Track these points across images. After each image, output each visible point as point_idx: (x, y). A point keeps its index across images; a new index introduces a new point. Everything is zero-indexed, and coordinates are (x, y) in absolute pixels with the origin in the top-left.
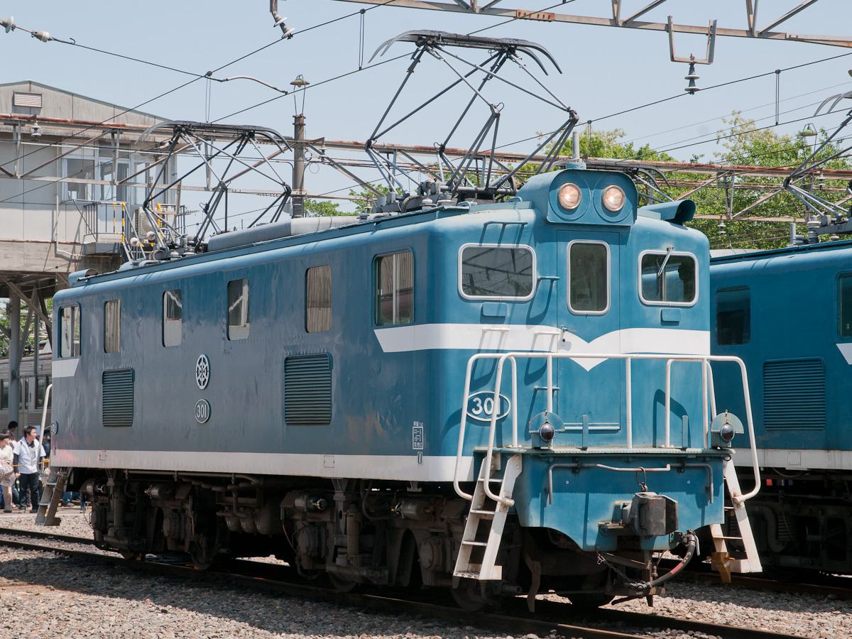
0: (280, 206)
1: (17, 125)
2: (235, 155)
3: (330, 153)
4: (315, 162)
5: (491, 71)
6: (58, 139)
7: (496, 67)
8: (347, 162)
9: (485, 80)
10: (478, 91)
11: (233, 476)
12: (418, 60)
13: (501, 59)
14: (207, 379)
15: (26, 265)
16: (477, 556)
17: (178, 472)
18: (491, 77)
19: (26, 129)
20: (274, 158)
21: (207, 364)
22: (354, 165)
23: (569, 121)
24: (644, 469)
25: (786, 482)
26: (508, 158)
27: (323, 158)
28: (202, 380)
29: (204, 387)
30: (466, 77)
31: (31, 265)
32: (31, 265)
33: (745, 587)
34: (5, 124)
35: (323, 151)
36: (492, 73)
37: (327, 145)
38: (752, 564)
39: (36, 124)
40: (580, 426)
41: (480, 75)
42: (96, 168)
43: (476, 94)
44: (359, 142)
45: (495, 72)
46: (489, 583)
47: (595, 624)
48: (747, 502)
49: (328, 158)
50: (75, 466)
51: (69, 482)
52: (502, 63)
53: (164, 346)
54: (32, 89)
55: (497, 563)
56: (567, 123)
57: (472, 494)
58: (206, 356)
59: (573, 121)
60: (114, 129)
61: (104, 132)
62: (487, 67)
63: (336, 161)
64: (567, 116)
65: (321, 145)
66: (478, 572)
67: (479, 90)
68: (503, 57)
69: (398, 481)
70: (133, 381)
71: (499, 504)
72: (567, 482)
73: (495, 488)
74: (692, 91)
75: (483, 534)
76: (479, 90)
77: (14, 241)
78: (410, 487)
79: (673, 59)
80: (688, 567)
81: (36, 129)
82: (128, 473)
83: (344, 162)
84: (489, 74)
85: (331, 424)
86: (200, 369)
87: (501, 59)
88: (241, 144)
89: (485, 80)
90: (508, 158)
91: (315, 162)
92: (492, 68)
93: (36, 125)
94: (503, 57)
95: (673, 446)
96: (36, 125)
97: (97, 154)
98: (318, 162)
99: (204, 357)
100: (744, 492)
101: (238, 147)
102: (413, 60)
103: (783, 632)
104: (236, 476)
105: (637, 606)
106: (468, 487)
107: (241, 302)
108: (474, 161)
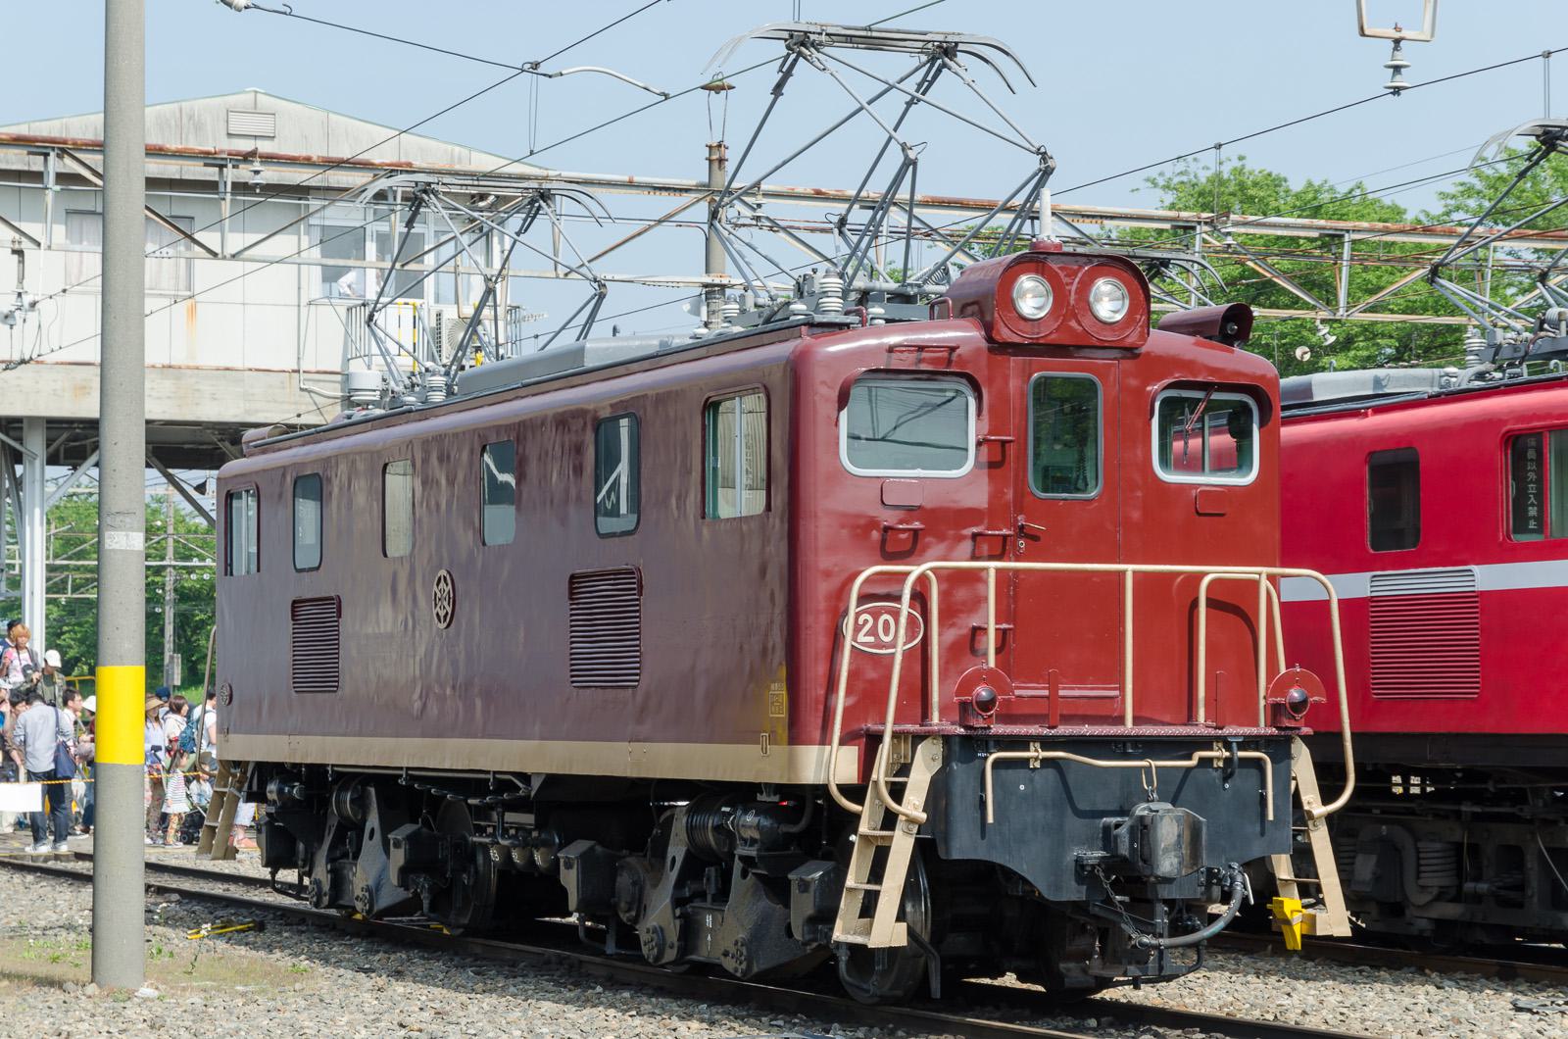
0: (585, 326)
1: (226, 166)
2: (518, 234)
3: (772, 208)
4: (744, 225)
5: (917, 91)
6: (301, 191)
7: (929, 78)
8: (802, 225)
9: (909, 104)
10: (893, 133)
11: (403, 773)
12: (787, 75)
13: (934, 69)
14: (449, 610)
15: (247, 412)
16: (868, 908)
17: (408, 769)
18: (919, 100)
19: (244, 174)
20: (673, 219)
21: (450, 586)
22: (813, 230)
23: (1040, 170)
24: (1153, 763)
25: (1406, 784)
26: (1088, 216)
27: (758, 218)
28: (442, 613)
29: (445, 624)
30: (869, 103)
31: (257, 411)
32: (257, 411)
33: (1323, 954)
34: (206, 165)
35: (759, 206)
36: (919, 95)
37: (766, 195)
38: (1335, 920)
39: (256, 164)
40: (1044, 688)
41: (896, 101)
42: (368, 244)
43: (890, 138)
44: (823, 190)
45: (924, 94)
46: (892, 952)
47: (997, 1015)
48: (1330, 818)
49: (768, 218)
50: (554, 771)
51: (250, 787)
52: (935, 78)
53: (385, 555)
54: (259, 105)
55: (266, 866)
56: (1036, 174)
57: (862, 804)
58: (449, 572)
59: (1046, 173)
60: (392, 171)
61: (375, 175)
62: (910, 85)
63: (783, 224)
64: (1034, 163)
65: (754, 195)
66: (868, 932)
67: (895, 130)
68: (937, 65)
69: (700, 781)
70: (339, 616)
71: (901, 818)
72: (1022, 787)
73: (897, 792)
74: (1397, 91)
75: (877, 873)
76: (895, 130)
77: (227, 369)
78: (762, 793)
79: (1363, 34)
80: (1234, 924)
81: (257, 172)
82: (333, 771)
83: (796, 224)
84: (913, 97)
85: (340, 692)
86: (439, 595)
87: (934, 69)
88: (528, 216)
89: (909, 104)
90: (1088, 216)
91: (744, 225)
92: (920, 85)
93: (257, 166)
94: (937, 65)
95: (1209, 723)
96: (257, 166)
97: (370, 217)
98: (750, 225)
99: (445, 573)
100: (1326, 801)
101: (525, 220)
102: (781, 74)
103: (1291, 1019)
104: (498, 776)
105: (1147, 995)
106: (856, 793)
107: (619, 476)
108: (1029, 222)
